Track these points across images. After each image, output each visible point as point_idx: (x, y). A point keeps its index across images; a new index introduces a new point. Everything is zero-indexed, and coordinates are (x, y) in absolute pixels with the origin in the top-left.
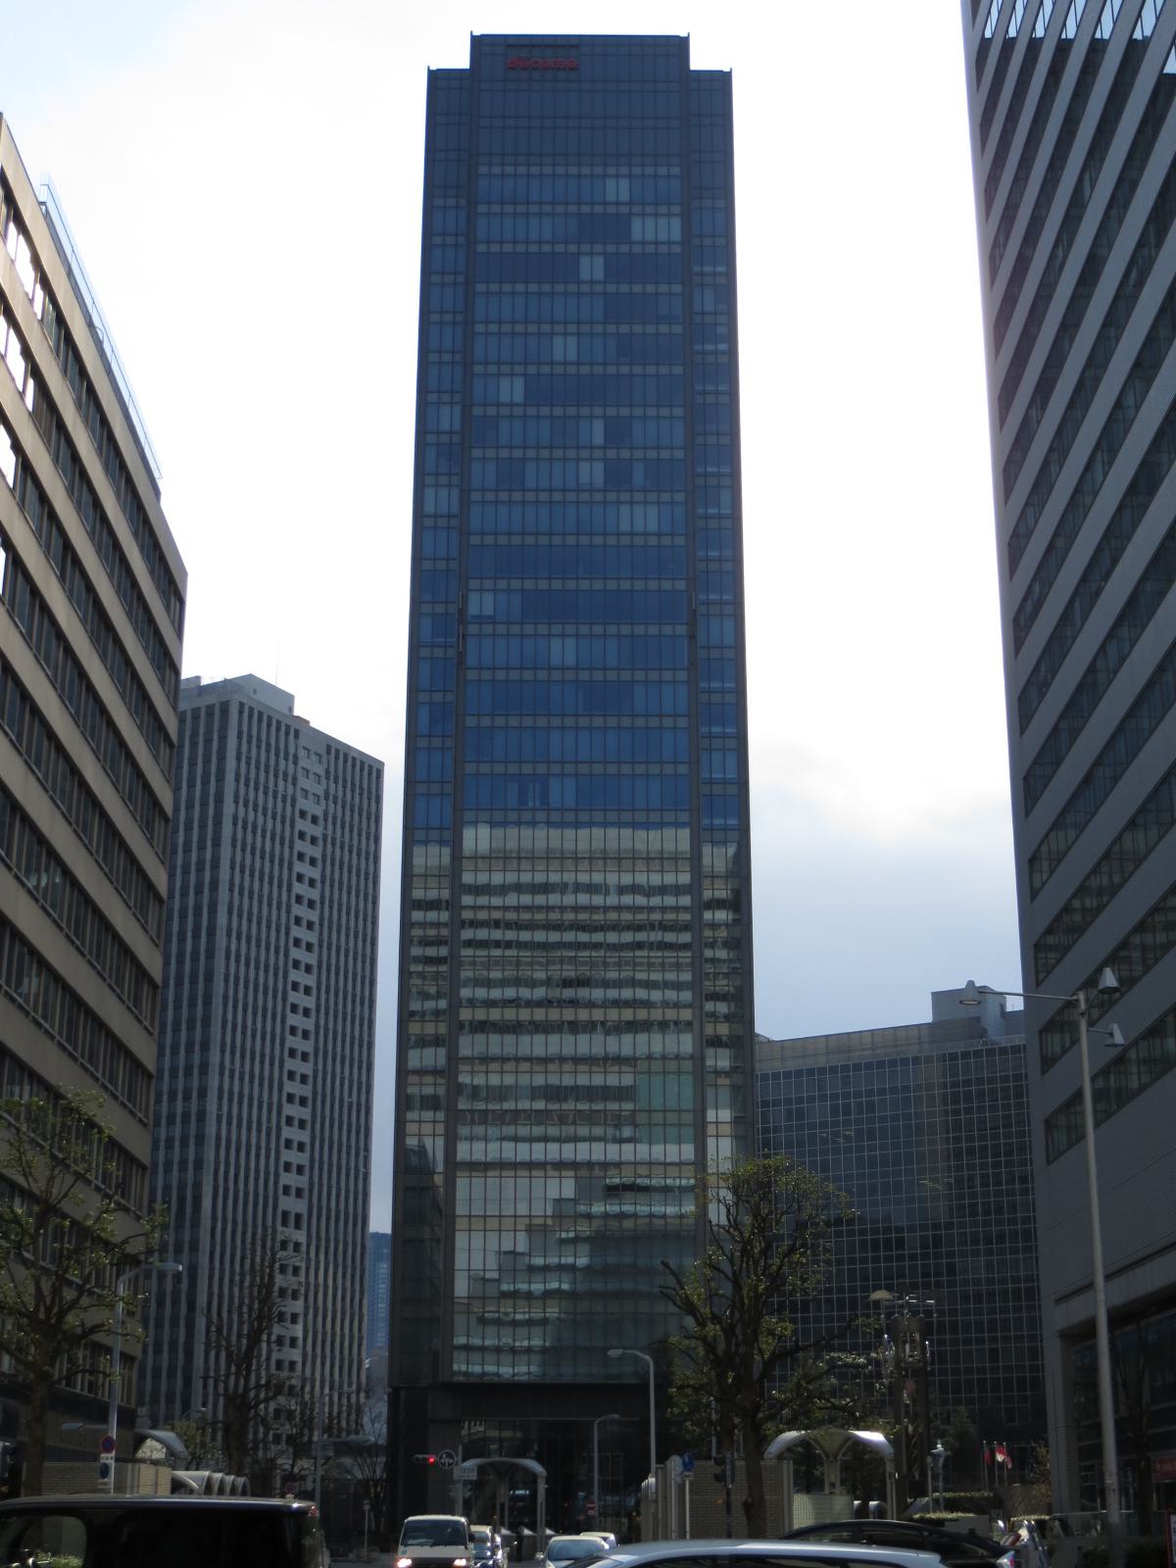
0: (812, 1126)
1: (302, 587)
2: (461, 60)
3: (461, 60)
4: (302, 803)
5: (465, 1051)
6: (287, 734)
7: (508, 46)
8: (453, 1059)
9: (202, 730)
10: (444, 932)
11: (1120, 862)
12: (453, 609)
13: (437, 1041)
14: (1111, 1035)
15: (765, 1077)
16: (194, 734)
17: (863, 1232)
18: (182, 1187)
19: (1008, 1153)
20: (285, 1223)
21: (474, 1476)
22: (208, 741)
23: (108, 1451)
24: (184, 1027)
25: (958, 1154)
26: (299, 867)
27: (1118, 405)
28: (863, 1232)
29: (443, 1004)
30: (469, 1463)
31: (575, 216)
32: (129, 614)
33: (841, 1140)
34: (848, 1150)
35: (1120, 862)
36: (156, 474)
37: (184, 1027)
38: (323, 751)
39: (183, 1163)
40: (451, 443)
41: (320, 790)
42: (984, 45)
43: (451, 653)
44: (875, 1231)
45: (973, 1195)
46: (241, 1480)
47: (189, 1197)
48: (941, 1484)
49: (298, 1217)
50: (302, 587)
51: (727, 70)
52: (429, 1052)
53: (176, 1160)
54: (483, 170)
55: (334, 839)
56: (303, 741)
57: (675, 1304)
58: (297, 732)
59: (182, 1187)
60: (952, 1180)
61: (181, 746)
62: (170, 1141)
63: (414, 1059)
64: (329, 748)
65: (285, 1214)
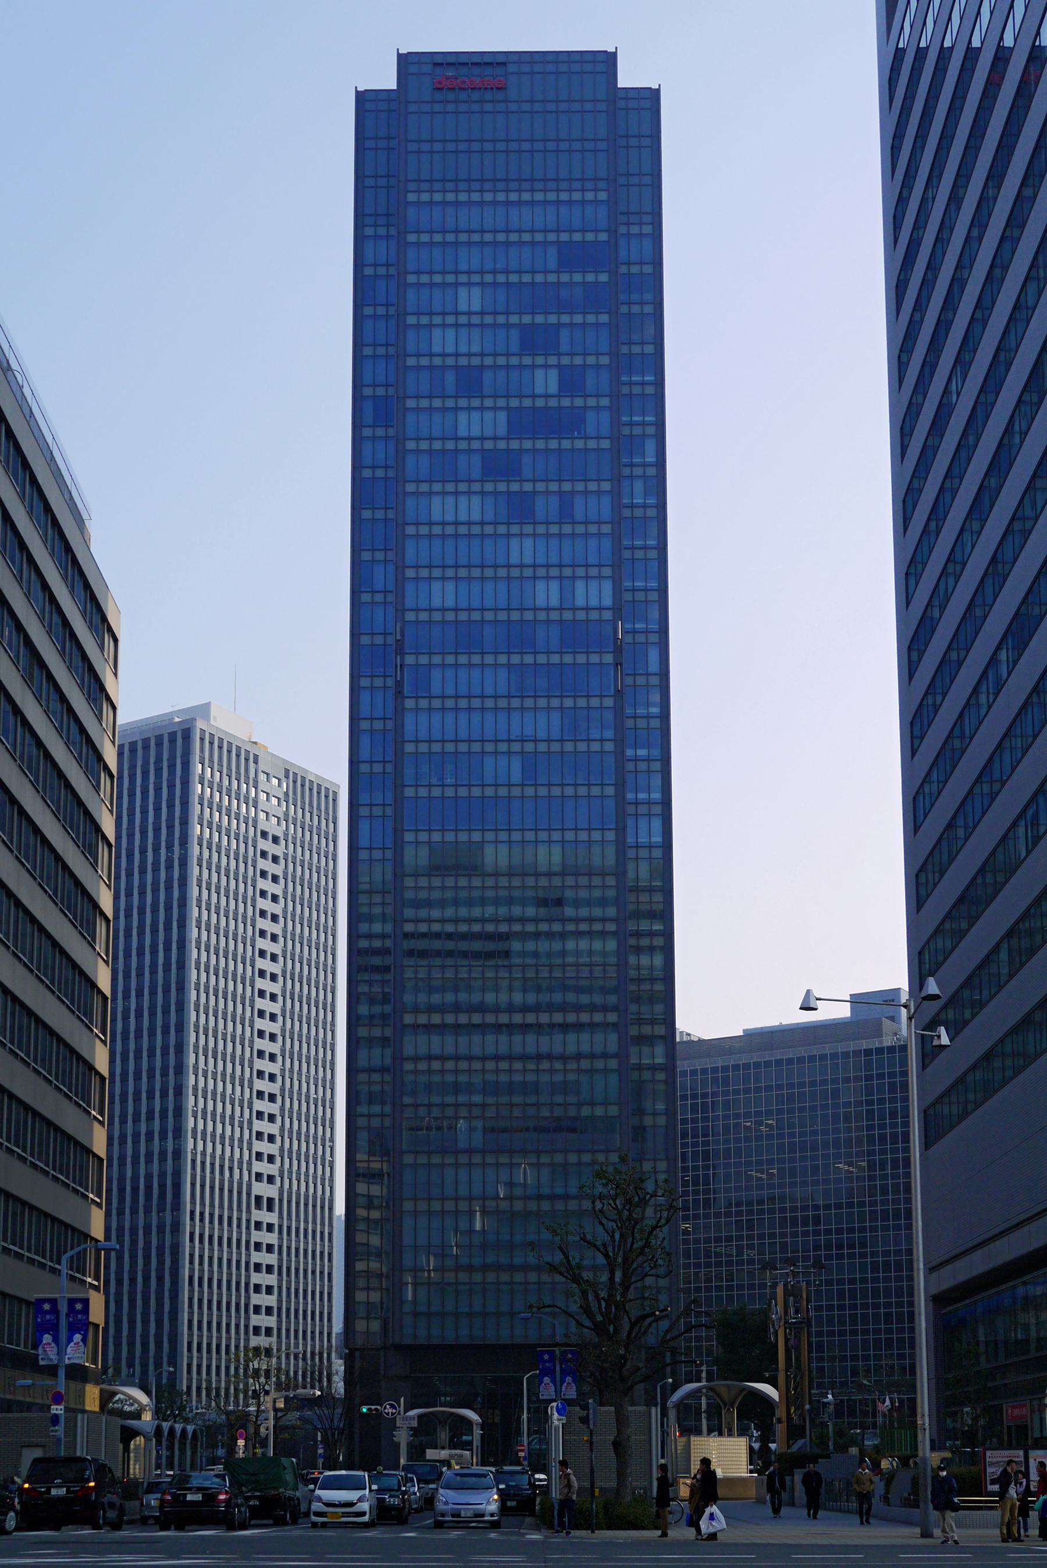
0: (737, 1116)
1: (234, 619)
2: (388, 81)
3: (388, 81)
4: (263, 825)
5: (409, 1050)
6: (247, 760)
7: (436, 64)
8: (399, 1058)
9: (139, 763)
10: (388, 943)
11: (997, 870)
12: (390, 640)
13: (384, 1041)
14: (939, 1037)
15: (684, 1074)
16: (133, 767)
17: (783, 1210)
18: (162, 1175)
19: (792, 1151)
20: (258, 1206)
21: (415, 1424)
22: (172, 767)
23: (58, 1403)
24: (159, 1031)
25: (706, 1156)
26: (262, 884)
27: (1008, 430)
28: (783, 1210)
29: (388, 1009)
30: (412, 1413)
31: (502, 239)
32: (62, 653)
33: (763, 1128)
34: (770, 1137)
35: (997, 870)
36: (85, 516)
37: (159, 1031)
38: (282, 776)
39: (163, 1154)
40: (386, 478)
41: (280, 812)
42: (899, 54)
43: (390, 682)
44: (794, 1209)
45: (884, 1177)
46: (958, 1443)
47: (128, 1188)
48: (293, 1417)
49: (270, 1200)
50: (234, 619)
51: (655, 86)
52: (377, 1052)
53: (156, 1151)
54: (411, 197)
55: (294, 858)
56: (262, 766)
57: (561, 1274)
58: (256, 757)
59: (162, 1175)
60: (865, 1164)
61: (120, 777)
62: (150, 1135)
63: (362, 1061)
64: (287, 771)
65: (258, 1199)
